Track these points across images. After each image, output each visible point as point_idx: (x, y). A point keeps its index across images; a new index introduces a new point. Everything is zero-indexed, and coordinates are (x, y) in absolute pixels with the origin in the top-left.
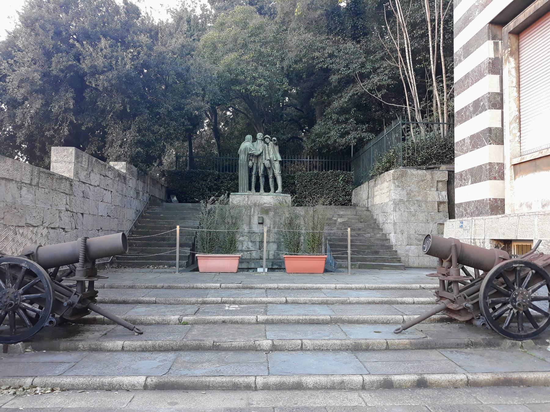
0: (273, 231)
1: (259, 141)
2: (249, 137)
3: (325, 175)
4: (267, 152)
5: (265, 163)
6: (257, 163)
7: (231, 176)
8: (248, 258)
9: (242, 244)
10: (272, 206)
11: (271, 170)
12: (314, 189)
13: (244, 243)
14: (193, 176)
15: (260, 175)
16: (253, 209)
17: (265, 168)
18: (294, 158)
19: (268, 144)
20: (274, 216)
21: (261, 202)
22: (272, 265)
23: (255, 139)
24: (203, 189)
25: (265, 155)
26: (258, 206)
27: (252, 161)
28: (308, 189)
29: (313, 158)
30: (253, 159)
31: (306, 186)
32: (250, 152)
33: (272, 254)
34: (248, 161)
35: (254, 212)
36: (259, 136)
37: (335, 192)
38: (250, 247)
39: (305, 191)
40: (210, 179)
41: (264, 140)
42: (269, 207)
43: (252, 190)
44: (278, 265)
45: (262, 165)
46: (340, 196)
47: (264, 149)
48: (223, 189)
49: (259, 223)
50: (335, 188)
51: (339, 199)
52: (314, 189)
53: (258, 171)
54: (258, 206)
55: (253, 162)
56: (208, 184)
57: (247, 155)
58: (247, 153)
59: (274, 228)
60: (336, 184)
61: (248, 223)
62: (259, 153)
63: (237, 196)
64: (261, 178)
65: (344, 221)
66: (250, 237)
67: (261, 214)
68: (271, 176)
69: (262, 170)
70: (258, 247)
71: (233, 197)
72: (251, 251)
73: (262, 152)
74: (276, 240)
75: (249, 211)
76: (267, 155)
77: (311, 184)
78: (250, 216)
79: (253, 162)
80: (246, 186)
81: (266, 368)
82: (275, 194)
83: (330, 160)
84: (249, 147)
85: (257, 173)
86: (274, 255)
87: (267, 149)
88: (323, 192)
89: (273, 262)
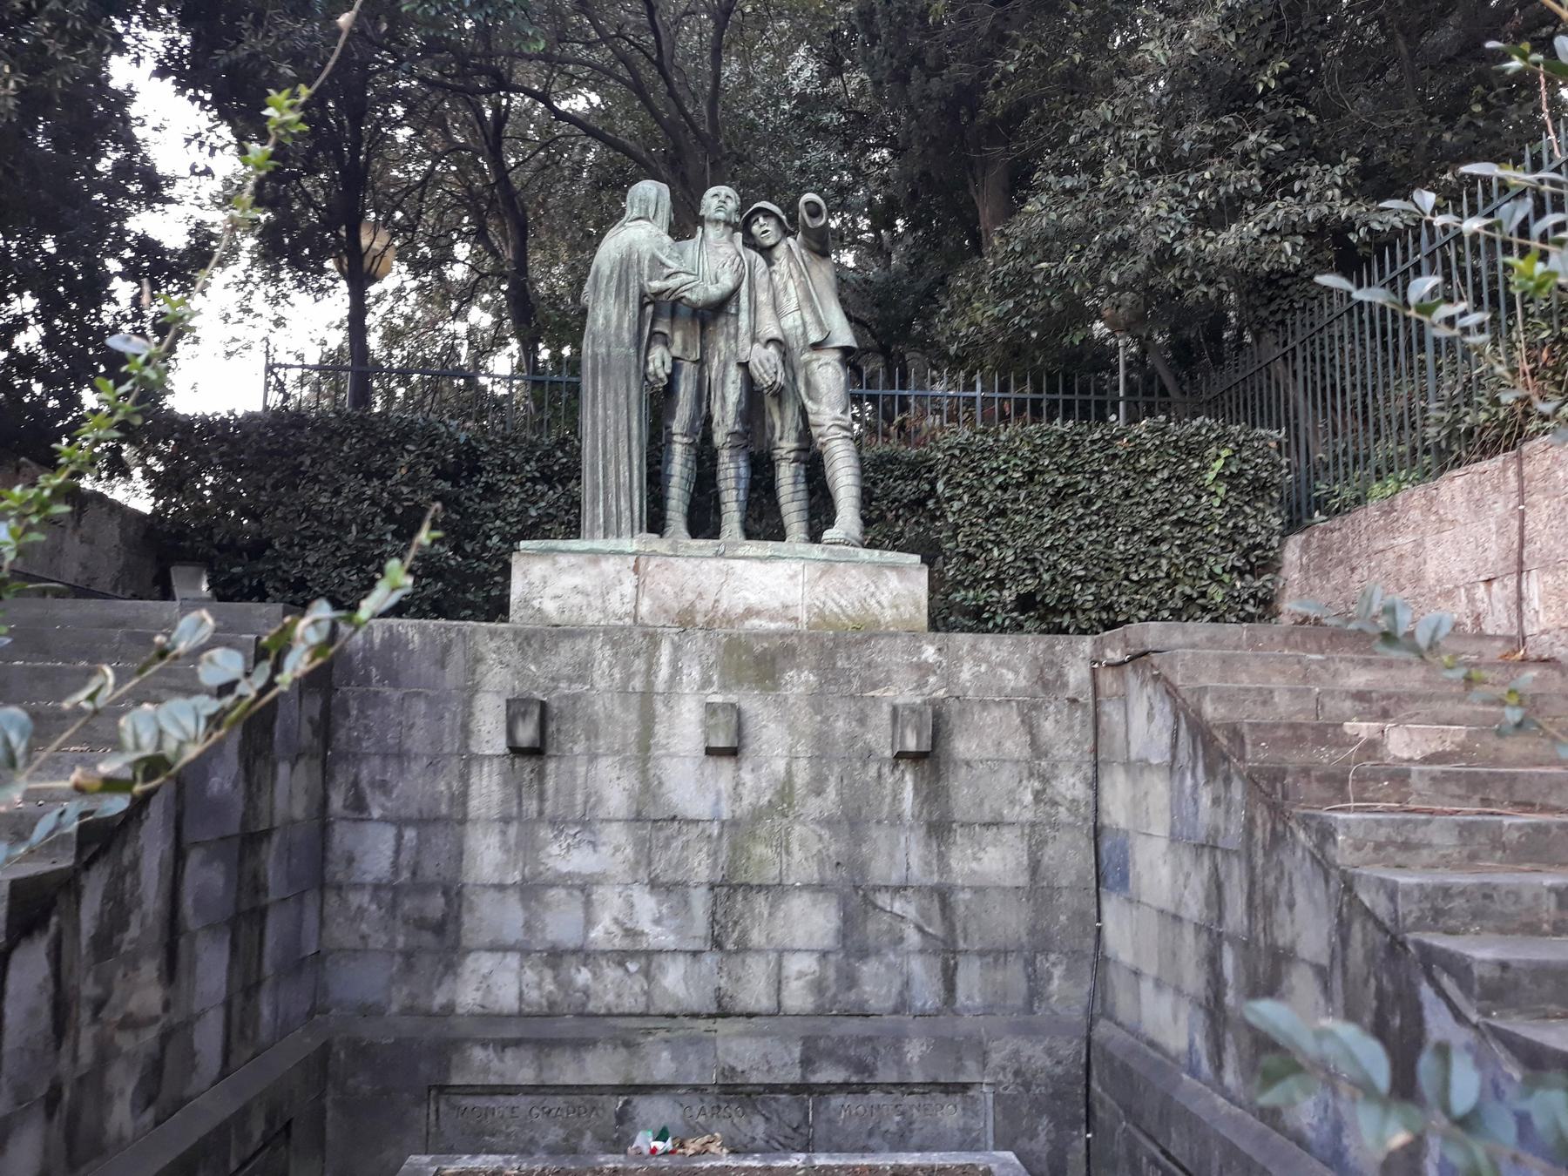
0: (814, 807)
1: (712, 232)
2: (649, 192)
3: (1121, 446)
4: (763, 297)
5: (754, 361)
6: (701, 363)
7: (548, 454)
8: (628, 1004)
9: (588, 904)
11: (791, 412)
12: (1051, 531)
13: (598, 893)
14: (300, 450)
15: (719, 438)
17: (754, 398)
19: (767, 252)
20: (817, 701)
21: (723, 605)
22: (806, 1062)
23: (685, 222)
24: (363, 529)
25: (754, 308)
26: (709, 626)
27: (667, 343)
29: (1004, 387)
30: (678, 337)
31: (1002, 513)
32: (656, 285)
33: (801, 975)
34: (642, 344)
35: (676, 671)
36: (715, 202)
37: (1184, 548)
38: (645, 925)
39: (999, 543)
40: (411, 467)
41: (743, 226)
42: (783, 635)
44: (846, 1062)
45: (734, 374)
46: (1212, 576)
47: (744, 275)
48: (499, 531)
49: (710, 751)
50: (1181, 523)
51: (1203, 595)
52: (1051, 531)
55: (676, 350)
57: (633, 306)
58: (634, 292)
59: (817, 786)
60: (1189, 499)
61: (633, 750)
62: (715, 291)
63: (563, 561)
64: (724, 456)
65: (1434, 747)
66: (644, 854)
67: (724, 687)
68: (787, 445)
69: (731, 407)
70: (701, 925)
71: (539, 569)
72: (649, 954)
73: (735, 291)
74: (829, 874)
75: (639, 664)
76: (766, 314)
78: (647, 696)
80: (633, 503)
82: (816, 551)
83: (1092, 396)
84: (646, 249)
85: (703, 425)
86: (818, 986)
87: (761, 279)
88: (1110, 545)
89: (809, 1043)
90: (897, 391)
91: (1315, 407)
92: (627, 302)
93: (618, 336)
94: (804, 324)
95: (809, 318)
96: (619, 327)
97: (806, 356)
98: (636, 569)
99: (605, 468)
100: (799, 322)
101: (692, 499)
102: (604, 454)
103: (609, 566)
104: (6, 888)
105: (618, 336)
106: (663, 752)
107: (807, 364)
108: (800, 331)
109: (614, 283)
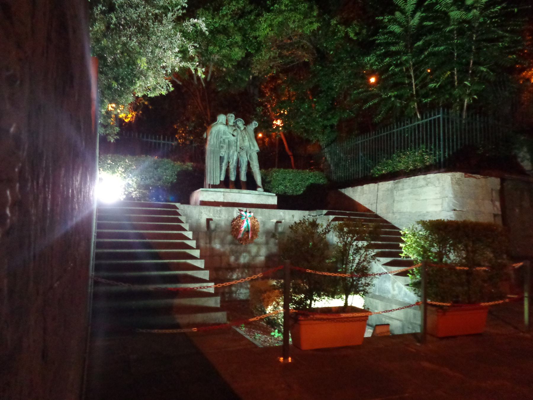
63: (210, 193)
90: (158, 141)
91: (160, 212)
93: (216, 146)
94: (250, 145)
95: (251, 143)
96: (216, 144)
98: (224, 195)
101: (443, 170)
103: (219, 194)
104: (206, 219)
105: (216, 146)
106: (339, 180)
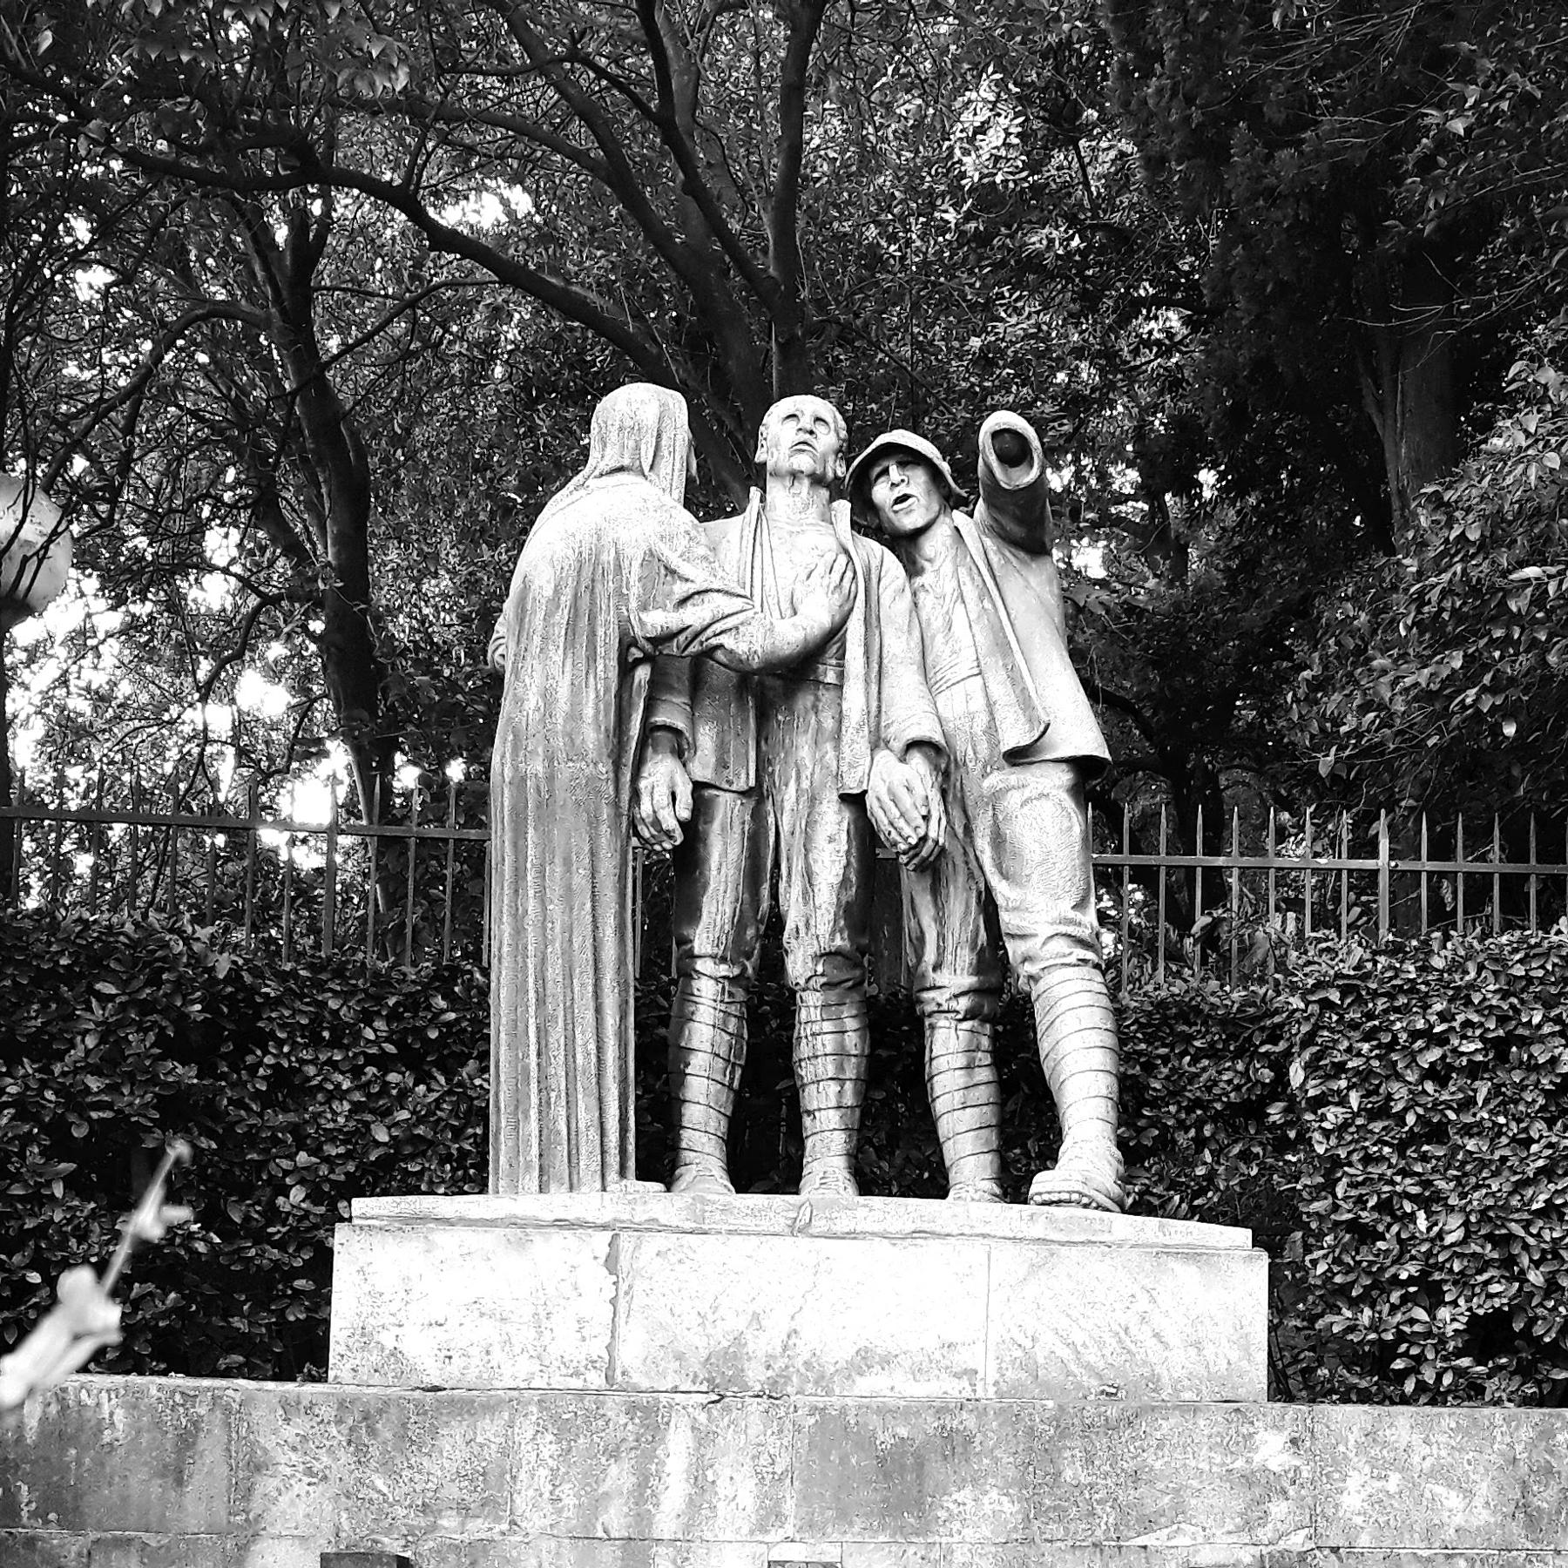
6: (758, 796)
7: (415, 1002)
10: (986, 1392)
11: (960, 904)
15: (799, 965)
16: (678, 1445)
18: (1213, 849)
19: (905, 545)
25: (877, 672)
26: (772, 1394)
28: (1470, 1172)
30: (706, 738)
31: (1438, 1133)
32: (657, 620)
35: (701, 1485)
39: (1430, 1201)
40: (107, 1032)
43: (687, 1175)
45: (833, 822)
48: (305, 1177)
53: (776, 922)
54: (772, 1394)
55: (702, 768)
56: (75, 1099)
57: (608, 667)
62: (790, 635)
63: (444, 1239)
64: (811, 1006)
73: (836, 633)
75: (619, 1476)
76: (903, 683)
77: (1503, 1100)
79: (702, 768)
81: (626, 462)
92: (592, 658)
96: (574, 716)
97: (994, 780)
99: (542, 1032)
100: (979, 703)
102: (541, 1001)
107: (996, 797)
108: (982, 720)
109: (562, 617)
